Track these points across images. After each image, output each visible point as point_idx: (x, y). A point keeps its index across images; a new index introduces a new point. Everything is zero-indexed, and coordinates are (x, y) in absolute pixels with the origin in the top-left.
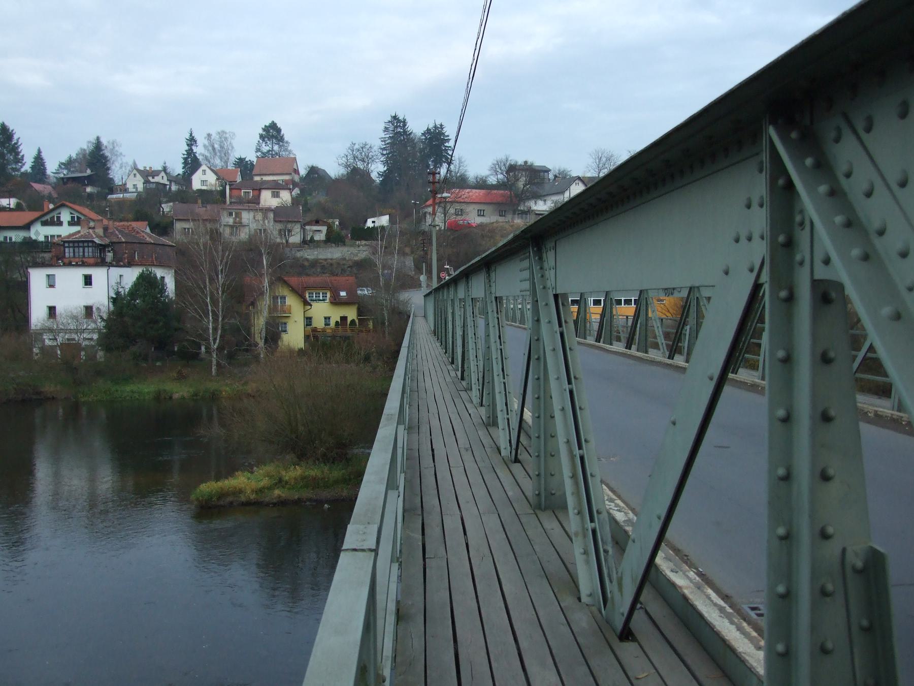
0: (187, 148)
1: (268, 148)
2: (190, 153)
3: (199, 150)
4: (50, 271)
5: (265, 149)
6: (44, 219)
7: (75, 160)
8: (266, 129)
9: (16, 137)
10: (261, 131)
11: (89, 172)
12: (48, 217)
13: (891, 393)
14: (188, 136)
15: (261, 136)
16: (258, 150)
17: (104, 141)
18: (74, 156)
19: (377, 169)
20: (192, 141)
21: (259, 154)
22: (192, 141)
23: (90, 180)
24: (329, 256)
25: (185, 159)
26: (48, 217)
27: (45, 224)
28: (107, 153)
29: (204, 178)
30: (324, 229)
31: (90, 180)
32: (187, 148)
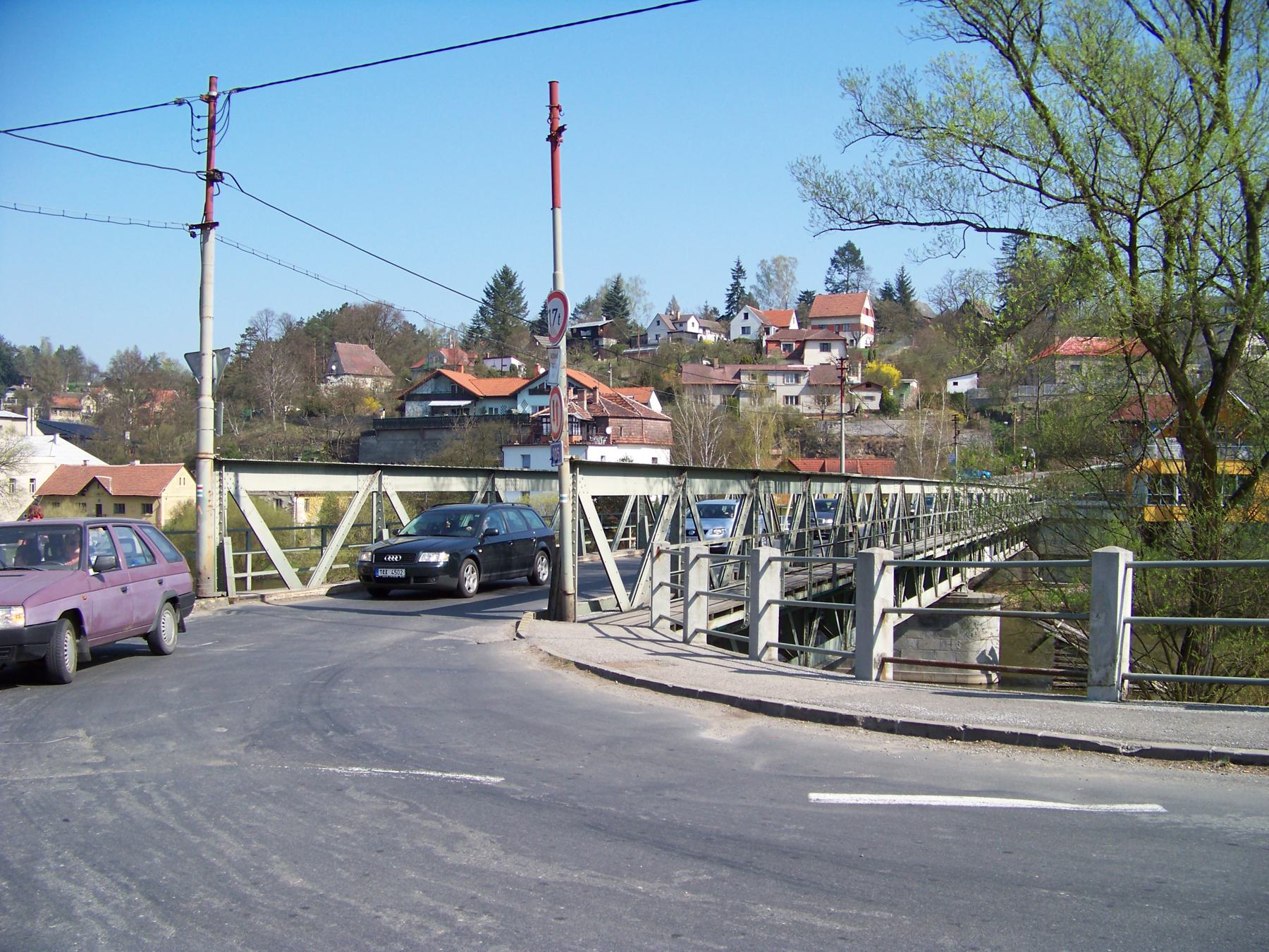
0: (733, 281)
1: (842, 278)
2: (736, 287)
3: (748, 284)
4: (526, 451)
5: (838, 278)
6: (533, 386)
7: (595, 302)
8: (840, 252)
9: (518, 281)
10: (833, 255)
11: (604, 321)
12: (536, 385)
13: (596, 505)
14: (734, 266)
15: (833, 261)
16: (828, 281)
17: (625, 279)
18: (594, 297)
19: (991, 300)
20: (739, 272)
21: (829, 285)
22: (739, 272)
23: (608, 331)
24: (876, 431)
25: (730, 296)
26: (536, 385)
27: (533, 392)
28: (626, 293)
29: (746, 324)
30: (878, 396)
31: (608, 331)
32: (733, 281)
